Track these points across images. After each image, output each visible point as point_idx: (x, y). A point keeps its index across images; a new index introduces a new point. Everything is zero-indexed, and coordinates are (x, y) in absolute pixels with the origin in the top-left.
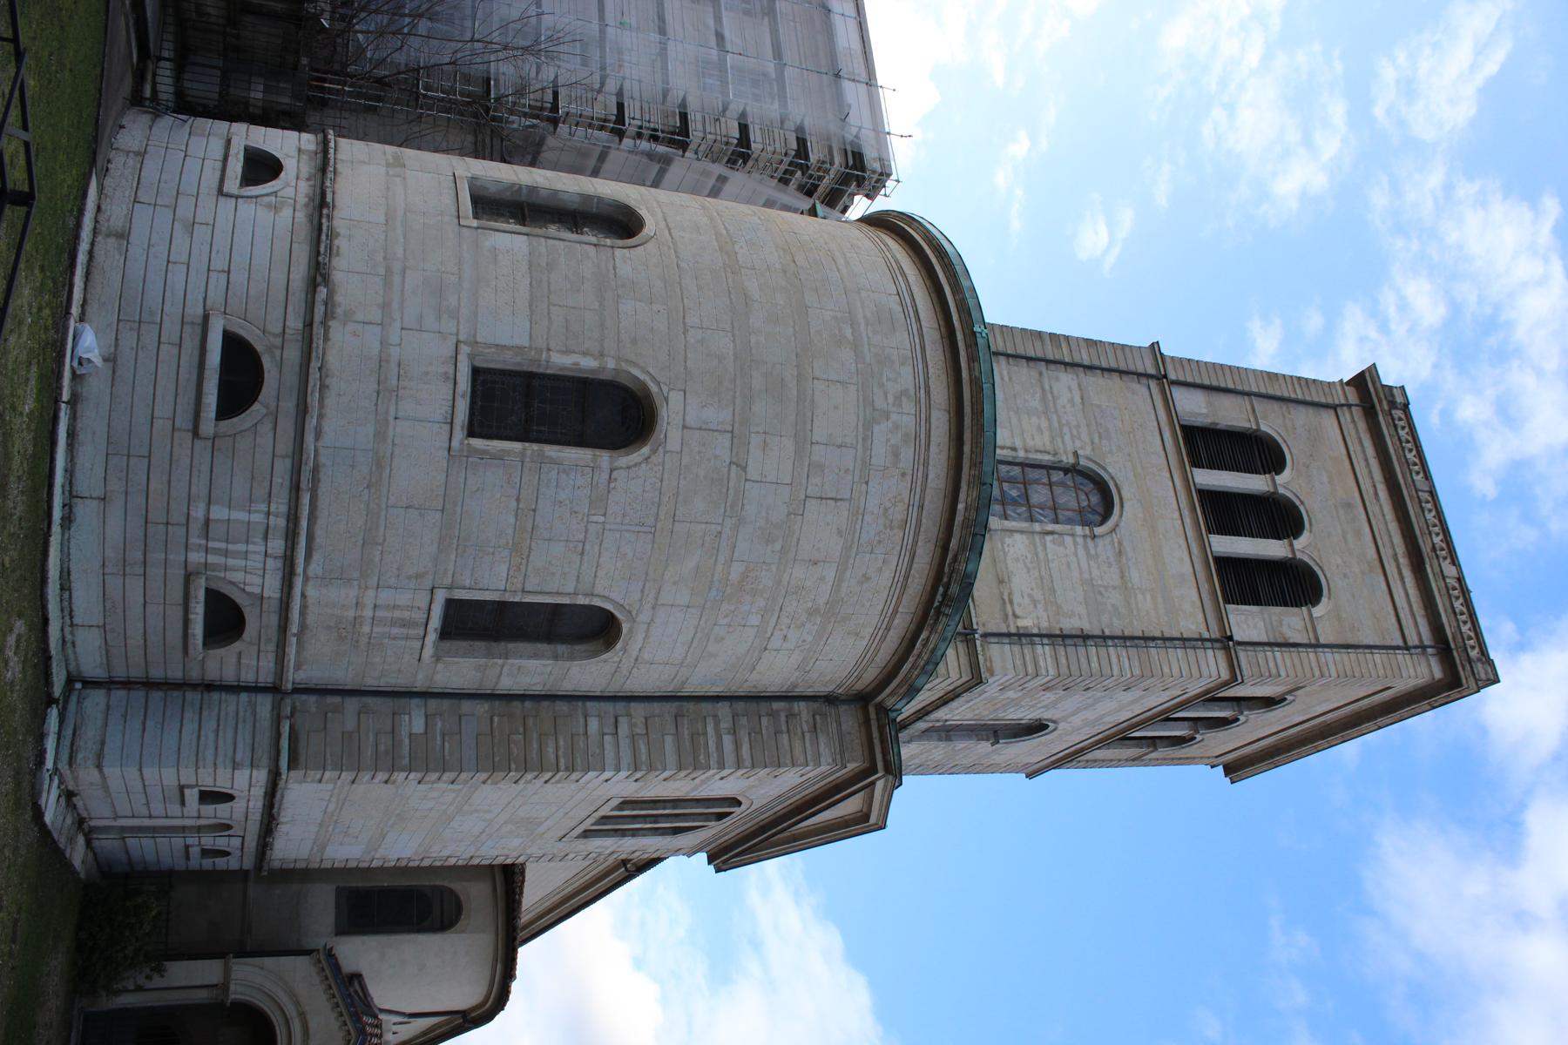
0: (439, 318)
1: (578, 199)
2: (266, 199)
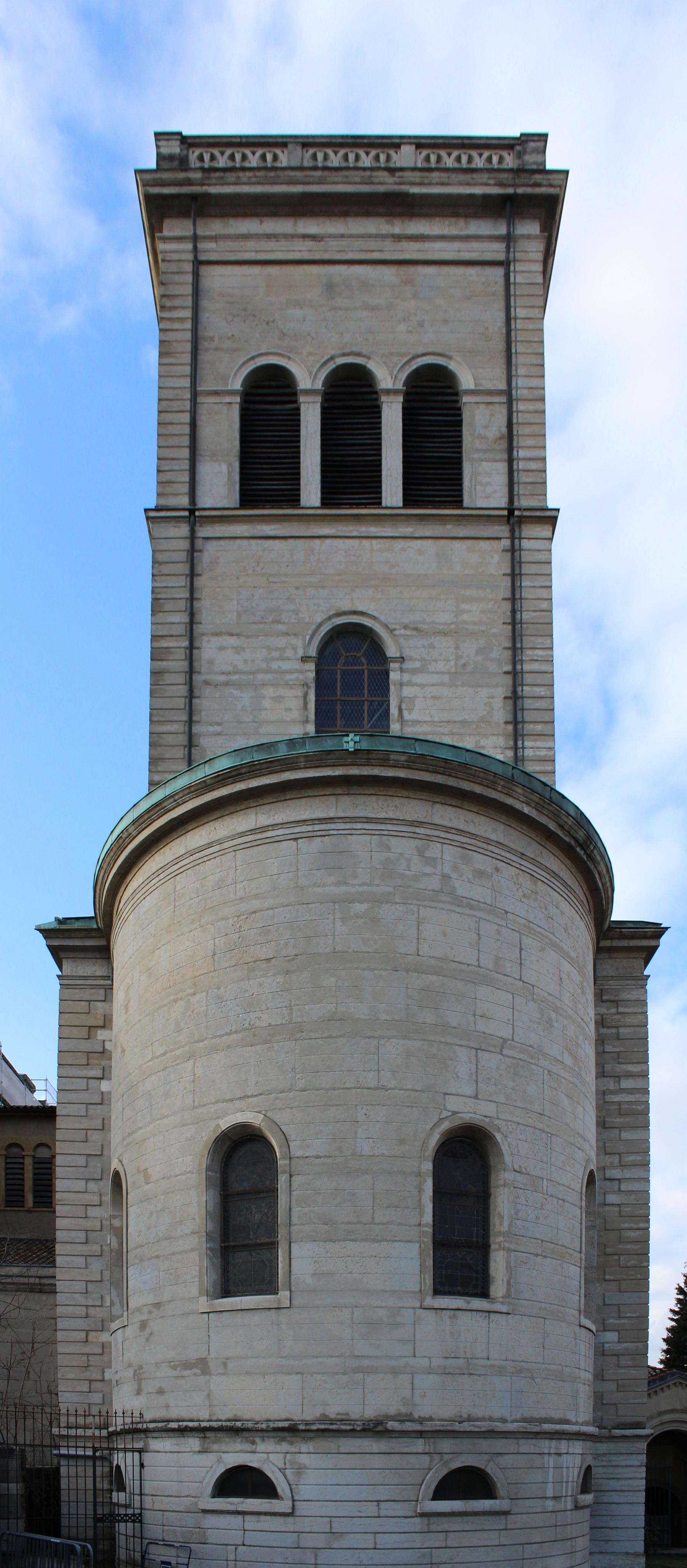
1: (211, 1191)
2: (290, 1477)
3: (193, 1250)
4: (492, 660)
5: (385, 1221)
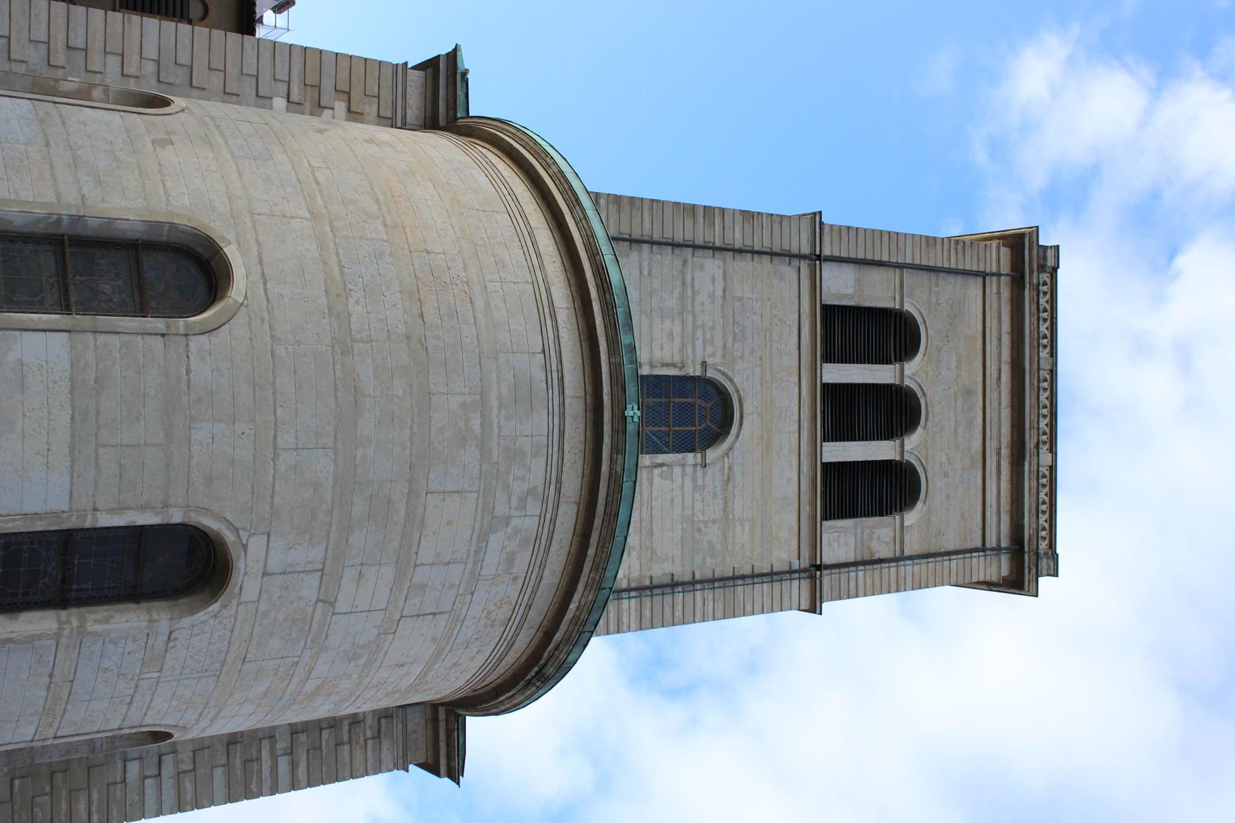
3: (58, 196)
4: (704, 558)
5: (101, 462)
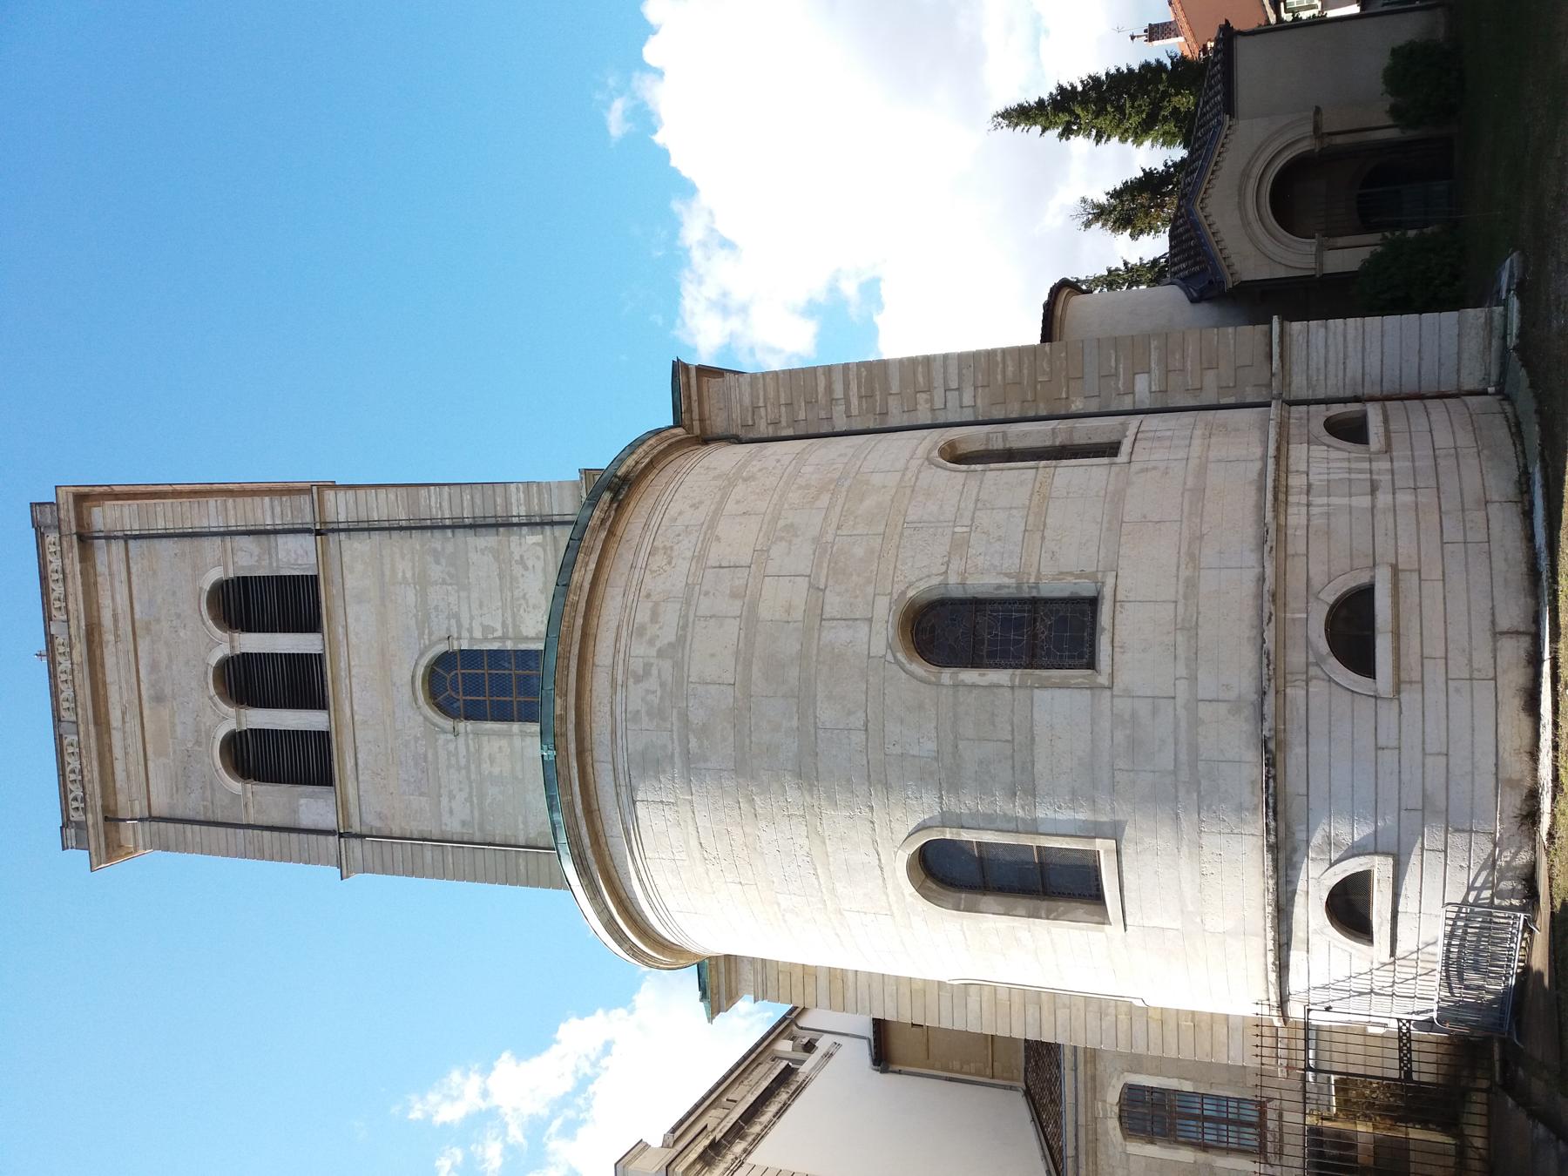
0: (1134, 715)
